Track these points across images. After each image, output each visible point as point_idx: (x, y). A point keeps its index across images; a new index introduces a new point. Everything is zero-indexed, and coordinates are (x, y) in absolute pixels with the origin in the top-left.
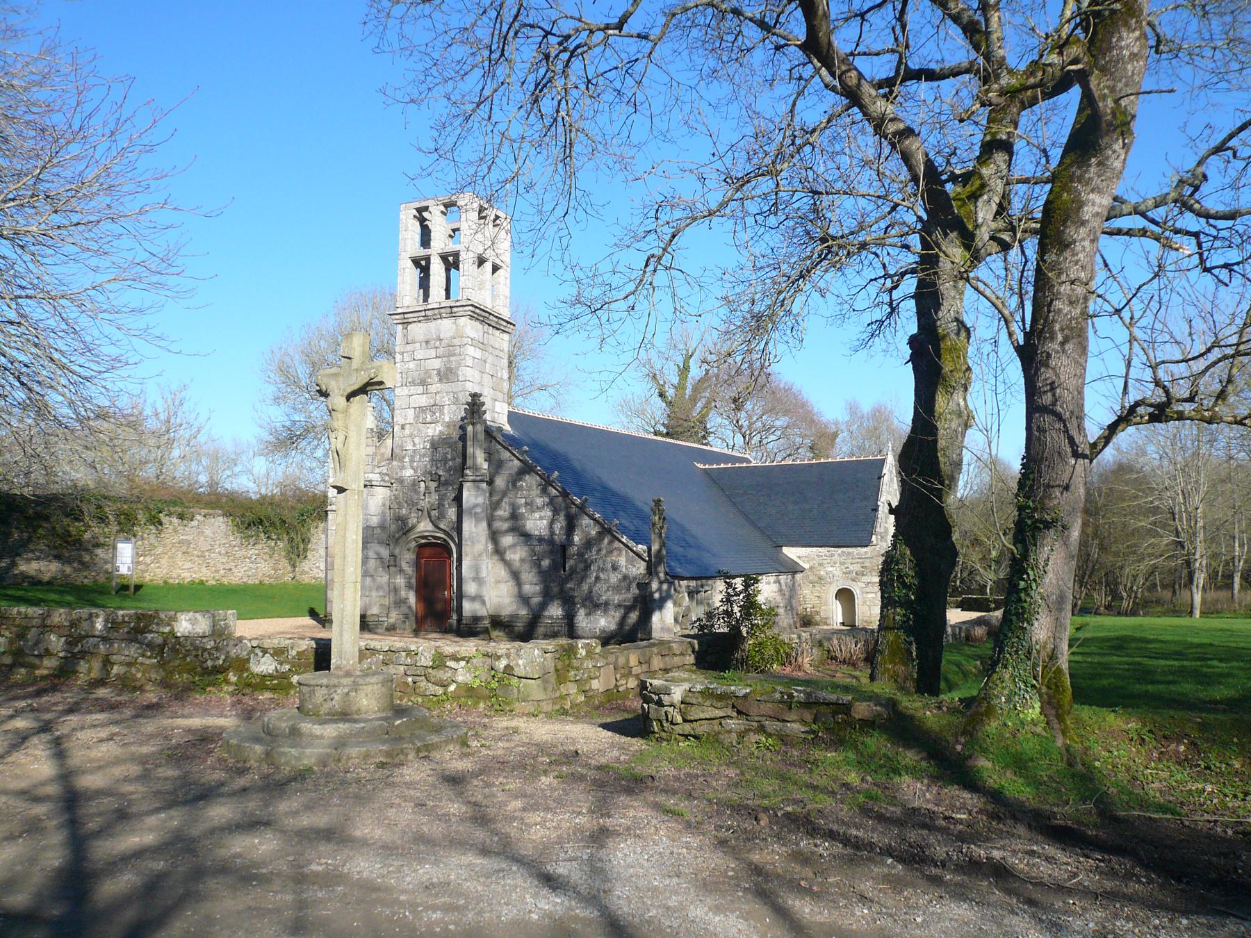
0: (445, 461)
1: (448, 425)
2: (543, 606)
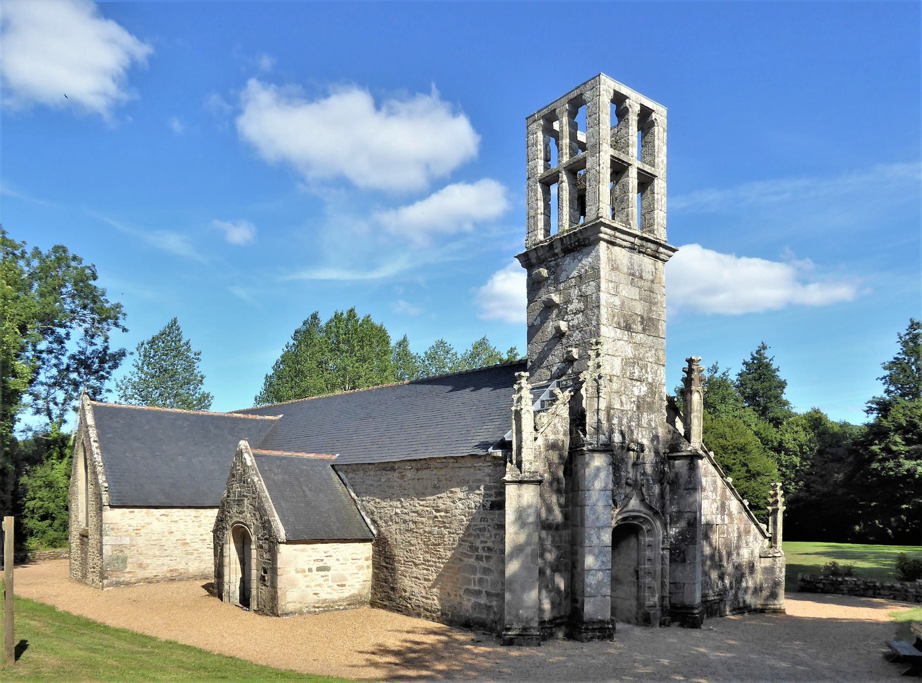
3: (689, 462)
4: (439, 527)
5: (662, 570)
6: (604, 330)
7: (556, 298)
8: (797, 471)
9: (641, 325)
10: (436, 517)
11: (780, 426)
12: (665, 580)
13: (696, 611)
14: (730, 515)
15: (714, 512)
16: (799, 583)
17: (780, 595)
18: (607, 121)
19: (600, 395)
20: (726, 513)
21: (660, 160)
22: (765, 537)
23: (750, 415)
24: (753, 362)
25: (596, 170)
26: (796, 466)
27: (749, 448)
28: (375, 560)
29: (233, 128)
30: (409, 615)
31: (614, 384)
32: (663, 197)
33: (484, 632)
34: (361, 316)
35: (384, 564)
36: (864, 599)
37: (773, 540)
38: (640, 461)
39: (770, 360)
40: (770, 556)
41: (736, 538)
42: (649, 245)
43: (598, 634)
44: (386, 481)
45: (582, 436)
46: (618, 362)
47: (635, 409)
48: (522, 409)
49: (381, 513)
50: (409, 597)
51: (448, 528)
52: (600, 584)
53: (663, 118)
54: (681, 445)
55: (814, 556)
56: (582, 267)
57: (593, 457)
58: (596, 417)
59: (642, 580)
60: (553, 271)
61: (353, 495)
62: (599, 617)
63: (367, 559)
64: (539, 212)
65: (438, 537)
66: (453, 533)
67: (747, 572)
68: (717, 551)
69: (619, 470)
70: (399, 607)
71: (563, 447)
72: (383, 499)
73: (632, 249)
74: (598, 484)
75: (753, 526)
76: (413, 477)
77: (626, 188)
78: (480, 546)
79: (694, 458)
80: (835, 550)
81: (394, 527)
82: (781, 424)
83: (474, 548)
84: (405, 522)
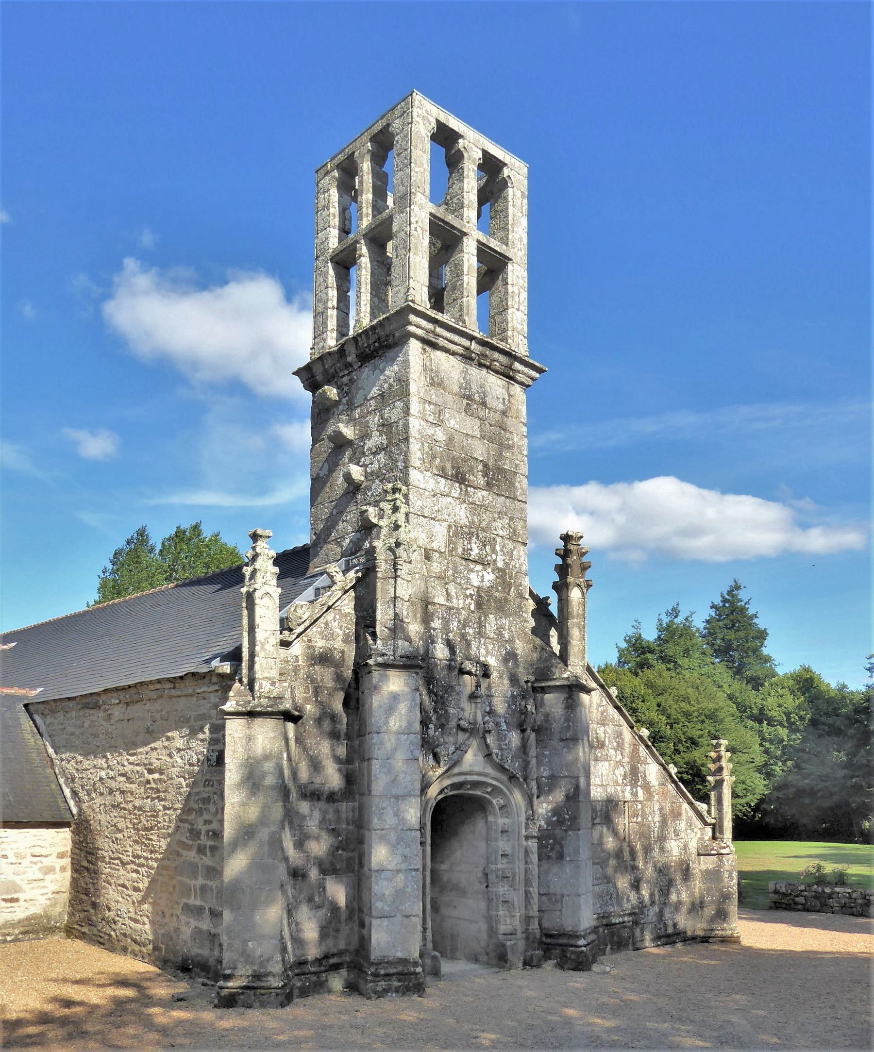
3: (566, 695)
4: (153, 799)
5: (526, 871)
6: (415, 476)
7: (348, 432)
8: (784, 747)
9: (484, 476)
10: (148, 782)
11: (760, 688)
12: (531, 889)
13: (582, 942)
14: (647, 787)
15: (620, 782)
16: (771, 895)
17: (731, 914)
18: (425, 162)
19: (399, 573)
20: (639, 783)
21: (517, 236)
22: (706, 824)
23: (720, 670)
24: (724, 605)
25: (406, 233)
26: (783, 741)
27: (720, 715)
28: (75, 857)
29: (98, 315)
30: (112, 950)
31: (435, 564)
32: (522, 290)
33: (206, 981)
34: (207, 533)
35: (85, 864)
36: (863, 920)
37: (717, 829)
38: (483, 690)
39: (746, 604)
40: (713, 852)
41: (657, 824)
42: (496, 355)
43: (396, 984)
44: (90, 726)
45: (371, 642)
46: (440, 531)
47: (472, 607)
48: (255, 590)
49: (82, 778)
50: (113, 920)
51: (162, 800)
52: (399, 894)
53: (522, 178)
54: (553, 669)
55: (805, 859)
56: (385, 381)
57: (386, 676)
58: (392, 611)
59: (494, 889)
60: (346, 391)
61: (51, 750)
62: (399, 955)
63: (61, 856)
64: (330, 305)
65: (151, 816)
66: (169, 809)
67: (678, 877)
68: (625, 844)
69: (443, 703)
70: (100, 937)
71: (343, 660)
72: (86, 755)
73: (467, 357)
74: (395, 723)
75: (685, 806)
76: (122, 717)
77: (460, 268)
78: (204, 829)
79: (574, 688)
80: (834, 852)
81: (99, 801)
82: (762, 685)
83: (195, 834)
84: (111, 792)
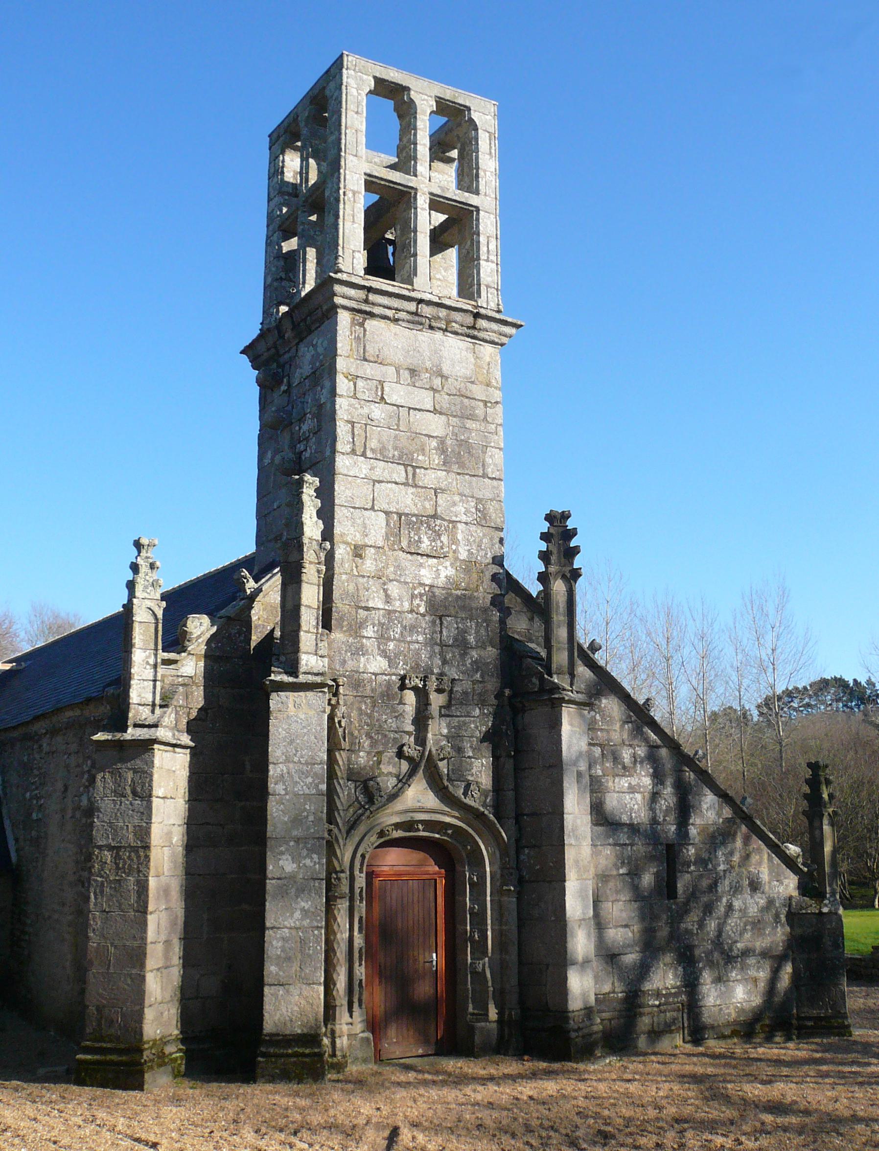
0: (461, 643)
1: (469, 566)
2: (643, 970)
47: (422, 610)
